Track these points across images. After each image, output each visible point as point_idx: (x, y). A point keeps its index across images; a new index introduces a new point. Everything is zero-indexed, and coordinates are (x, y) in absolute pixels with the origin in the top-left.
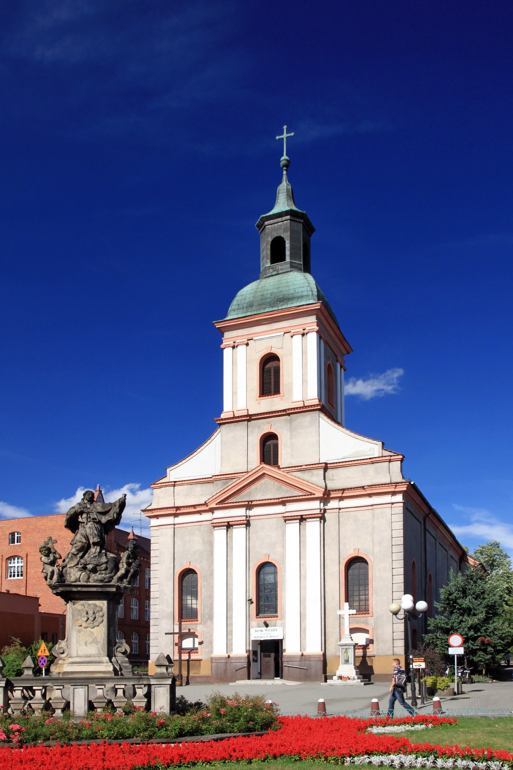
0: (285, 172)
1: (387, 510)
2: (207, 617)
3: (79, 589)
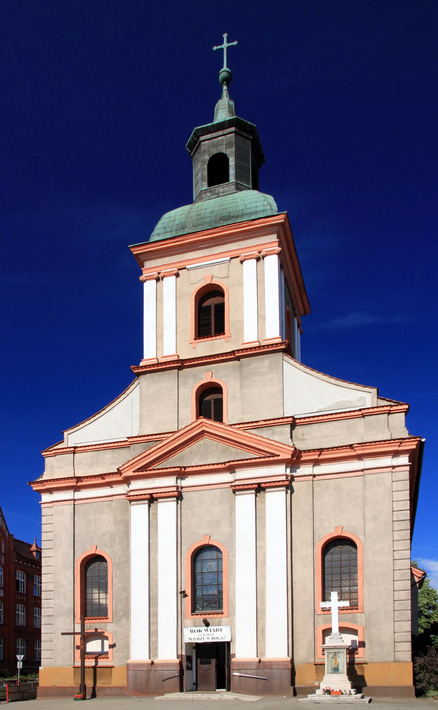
0: (225, 88)
1: (387, 476)
2: (121, 613)
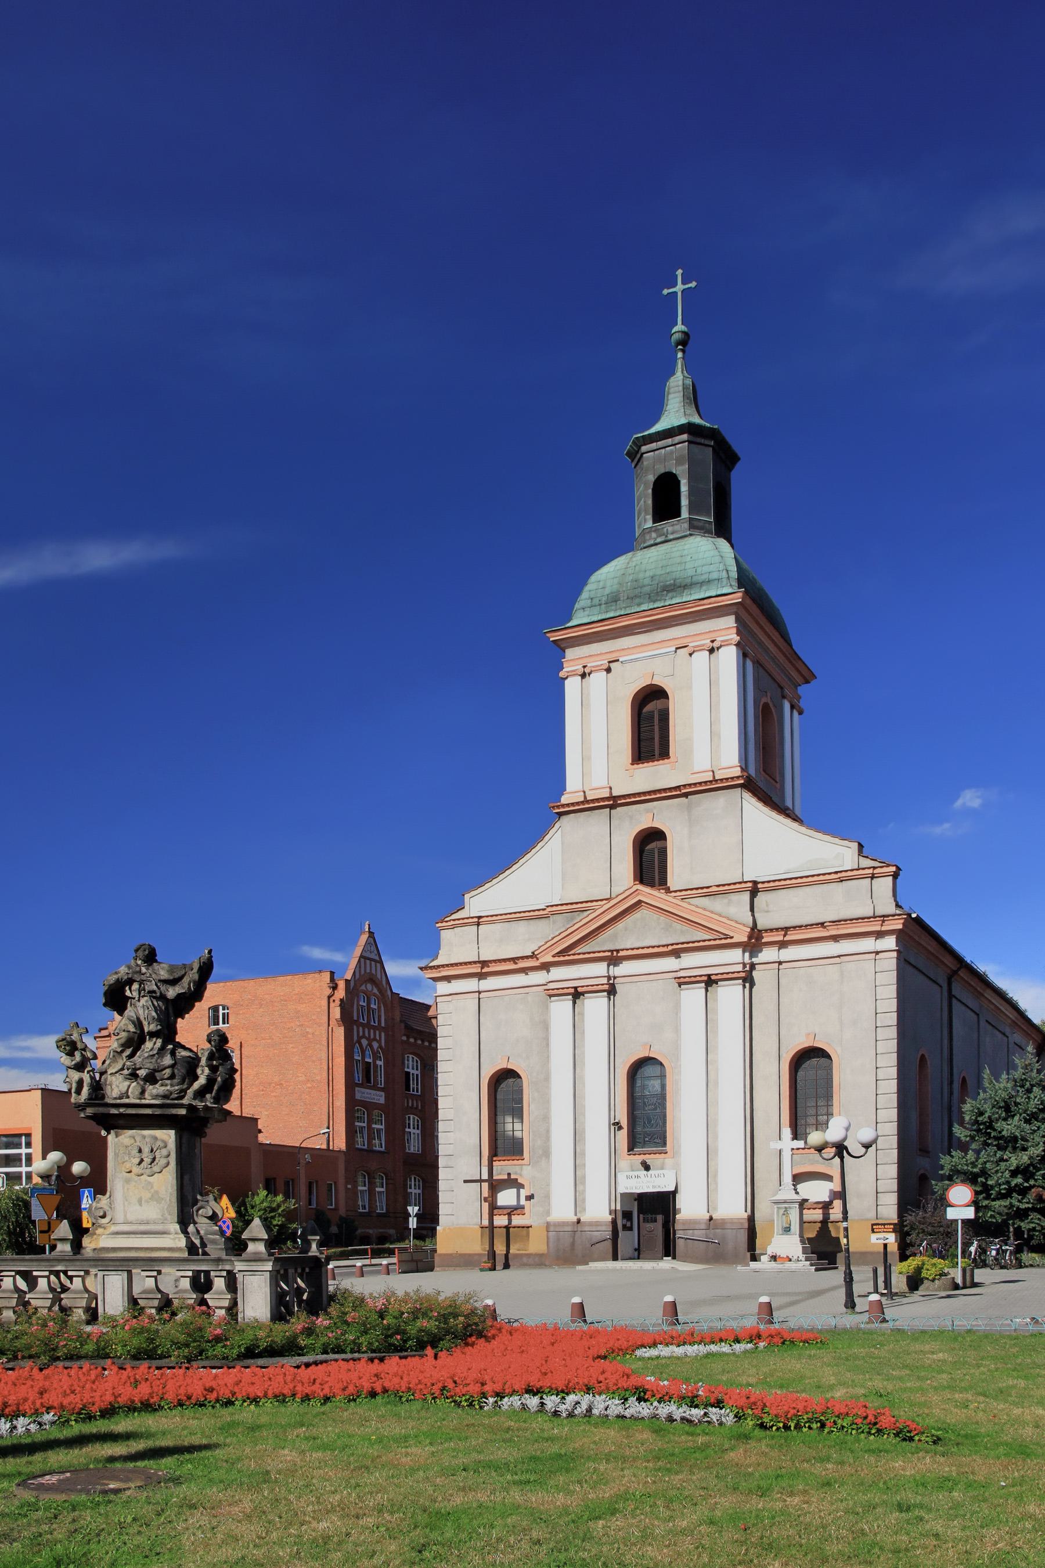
1: (867, 965)
3: (122, 1110)
